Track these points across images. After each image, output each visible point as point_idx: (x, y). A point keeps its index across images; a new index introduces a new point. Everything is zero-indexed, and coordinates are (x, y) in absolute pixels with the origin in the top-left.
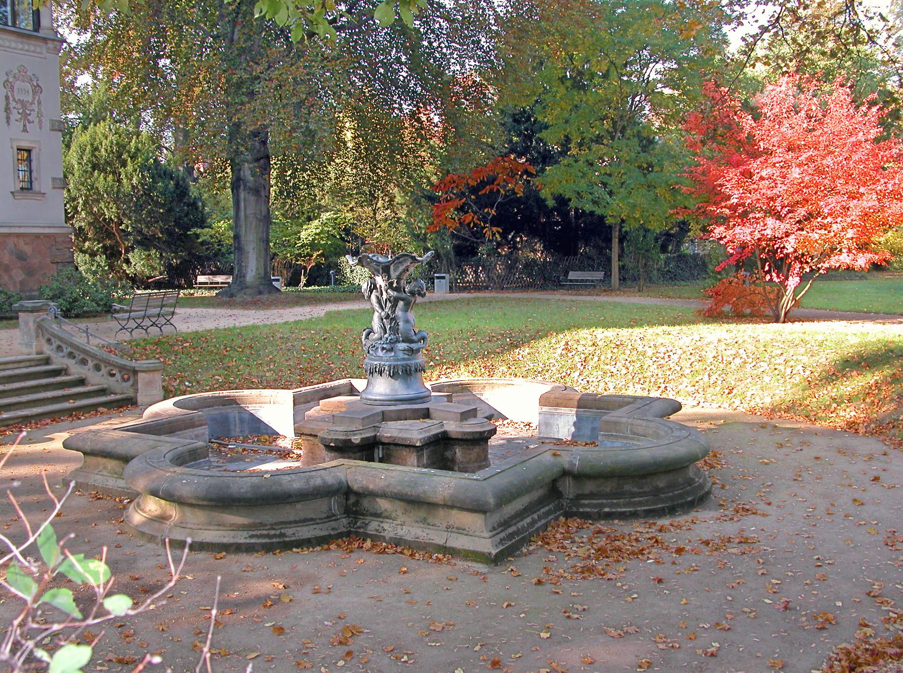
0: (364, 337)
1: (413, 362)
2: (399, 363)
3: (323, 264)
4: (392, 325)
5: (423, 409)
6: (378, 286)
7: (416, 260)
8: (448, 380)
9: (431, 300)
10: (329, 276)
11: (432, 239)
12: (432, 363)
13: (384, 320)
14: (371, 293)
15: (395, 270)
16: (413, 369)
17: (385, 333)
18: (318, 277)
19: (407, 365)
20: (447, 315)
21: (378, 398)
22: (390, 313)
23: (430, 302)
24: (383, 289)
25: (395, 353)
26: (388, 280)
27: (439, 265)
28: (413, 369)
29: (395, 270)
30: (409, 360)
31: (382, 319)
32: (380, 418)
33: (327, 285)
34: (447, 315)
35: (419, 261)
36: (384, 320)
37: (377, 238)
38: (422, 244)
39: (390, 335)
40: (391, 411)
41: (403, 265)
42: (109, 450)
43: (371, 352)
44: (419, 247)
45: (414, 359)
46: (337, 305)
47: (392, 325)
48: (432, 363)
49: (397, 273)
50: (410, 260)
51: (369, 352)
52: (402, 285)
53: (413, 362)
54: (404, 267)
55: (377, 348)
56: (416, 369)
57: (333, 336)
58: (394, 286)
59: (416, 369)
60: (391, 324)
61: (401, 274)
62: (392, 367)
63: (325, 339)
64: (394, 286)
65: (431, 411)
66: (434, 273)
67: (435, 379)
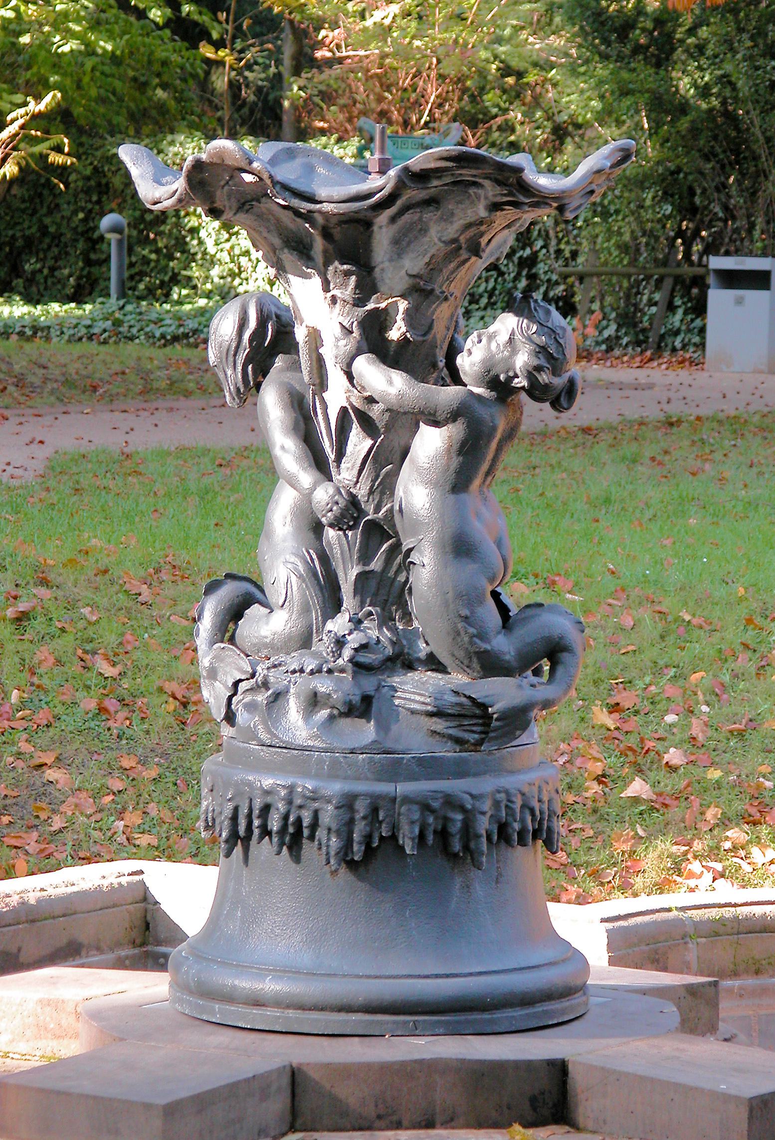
0: (206, 625)
1: (486, 785)
2: (403, 788)
3: (62, 171)
4: (376, 564)
5: (528, 1066)
6: (300, 334)
7: (525, 188)
8: (726, 891)
9: (675, 410)
10: (96, 242)
11: (701, 48)
12: (638, 787)
13: (331, 534)
14: (263, 371)
15: (400, 245)
16: (483, 824)
17: (333, 605)
18: (30, 244)
19: (450, 801)
20: (752, 505)
21: (270, 986)
22: (361, 492)
23: (671, 424)
24: (328, 352)
25: (383, 727)
26: (359, 302)
27: (737, 200)
28: (483, 824)
29: (400, 245)
30: (460, 771)
31: (317, 528)
32: (278, 1104)
33: (78, 297)
34: (752, 505)
35: (540, 199)
36: (331, 534)
37: (384, 31)
38: (645, 75)
39: (357, 623)
40: (346, 1071)
41: (448, 218)
42: (552, 960)
43: (242, 717)
44: (625, 92)
45: (498, 770)
46: (124, 421)
47: (376, 564)
48: (638, 787)
49: (414, 263)
50: (490, 191)
51: (230, 717)
52: (440, 332)
53: (486, 785)
54: (452, 231)
55: (278, 696)
56: (503, 829)
57: (71, 605)
58: (395, 334)
59: (503, 829)
60: (365, 556)
61: (433, 268)
62: (361, 808)
63: (21, 619)
64: (395, 334)
65: (578, 1078)
66: (711, 249)
67: (652, 876)
